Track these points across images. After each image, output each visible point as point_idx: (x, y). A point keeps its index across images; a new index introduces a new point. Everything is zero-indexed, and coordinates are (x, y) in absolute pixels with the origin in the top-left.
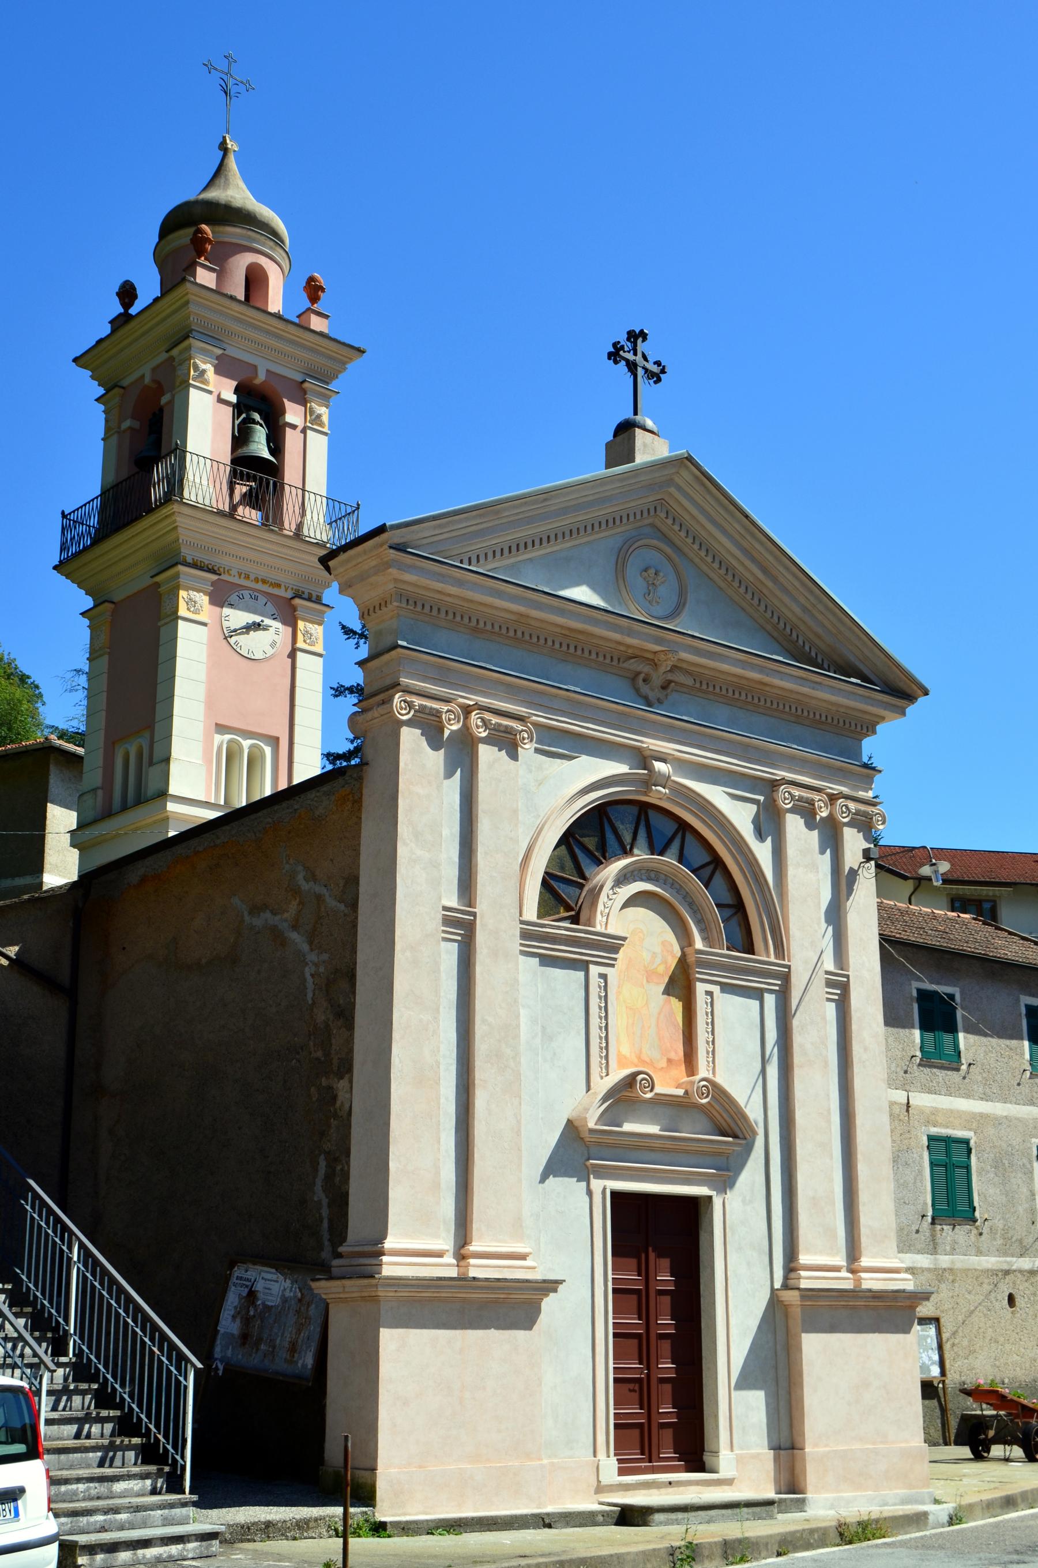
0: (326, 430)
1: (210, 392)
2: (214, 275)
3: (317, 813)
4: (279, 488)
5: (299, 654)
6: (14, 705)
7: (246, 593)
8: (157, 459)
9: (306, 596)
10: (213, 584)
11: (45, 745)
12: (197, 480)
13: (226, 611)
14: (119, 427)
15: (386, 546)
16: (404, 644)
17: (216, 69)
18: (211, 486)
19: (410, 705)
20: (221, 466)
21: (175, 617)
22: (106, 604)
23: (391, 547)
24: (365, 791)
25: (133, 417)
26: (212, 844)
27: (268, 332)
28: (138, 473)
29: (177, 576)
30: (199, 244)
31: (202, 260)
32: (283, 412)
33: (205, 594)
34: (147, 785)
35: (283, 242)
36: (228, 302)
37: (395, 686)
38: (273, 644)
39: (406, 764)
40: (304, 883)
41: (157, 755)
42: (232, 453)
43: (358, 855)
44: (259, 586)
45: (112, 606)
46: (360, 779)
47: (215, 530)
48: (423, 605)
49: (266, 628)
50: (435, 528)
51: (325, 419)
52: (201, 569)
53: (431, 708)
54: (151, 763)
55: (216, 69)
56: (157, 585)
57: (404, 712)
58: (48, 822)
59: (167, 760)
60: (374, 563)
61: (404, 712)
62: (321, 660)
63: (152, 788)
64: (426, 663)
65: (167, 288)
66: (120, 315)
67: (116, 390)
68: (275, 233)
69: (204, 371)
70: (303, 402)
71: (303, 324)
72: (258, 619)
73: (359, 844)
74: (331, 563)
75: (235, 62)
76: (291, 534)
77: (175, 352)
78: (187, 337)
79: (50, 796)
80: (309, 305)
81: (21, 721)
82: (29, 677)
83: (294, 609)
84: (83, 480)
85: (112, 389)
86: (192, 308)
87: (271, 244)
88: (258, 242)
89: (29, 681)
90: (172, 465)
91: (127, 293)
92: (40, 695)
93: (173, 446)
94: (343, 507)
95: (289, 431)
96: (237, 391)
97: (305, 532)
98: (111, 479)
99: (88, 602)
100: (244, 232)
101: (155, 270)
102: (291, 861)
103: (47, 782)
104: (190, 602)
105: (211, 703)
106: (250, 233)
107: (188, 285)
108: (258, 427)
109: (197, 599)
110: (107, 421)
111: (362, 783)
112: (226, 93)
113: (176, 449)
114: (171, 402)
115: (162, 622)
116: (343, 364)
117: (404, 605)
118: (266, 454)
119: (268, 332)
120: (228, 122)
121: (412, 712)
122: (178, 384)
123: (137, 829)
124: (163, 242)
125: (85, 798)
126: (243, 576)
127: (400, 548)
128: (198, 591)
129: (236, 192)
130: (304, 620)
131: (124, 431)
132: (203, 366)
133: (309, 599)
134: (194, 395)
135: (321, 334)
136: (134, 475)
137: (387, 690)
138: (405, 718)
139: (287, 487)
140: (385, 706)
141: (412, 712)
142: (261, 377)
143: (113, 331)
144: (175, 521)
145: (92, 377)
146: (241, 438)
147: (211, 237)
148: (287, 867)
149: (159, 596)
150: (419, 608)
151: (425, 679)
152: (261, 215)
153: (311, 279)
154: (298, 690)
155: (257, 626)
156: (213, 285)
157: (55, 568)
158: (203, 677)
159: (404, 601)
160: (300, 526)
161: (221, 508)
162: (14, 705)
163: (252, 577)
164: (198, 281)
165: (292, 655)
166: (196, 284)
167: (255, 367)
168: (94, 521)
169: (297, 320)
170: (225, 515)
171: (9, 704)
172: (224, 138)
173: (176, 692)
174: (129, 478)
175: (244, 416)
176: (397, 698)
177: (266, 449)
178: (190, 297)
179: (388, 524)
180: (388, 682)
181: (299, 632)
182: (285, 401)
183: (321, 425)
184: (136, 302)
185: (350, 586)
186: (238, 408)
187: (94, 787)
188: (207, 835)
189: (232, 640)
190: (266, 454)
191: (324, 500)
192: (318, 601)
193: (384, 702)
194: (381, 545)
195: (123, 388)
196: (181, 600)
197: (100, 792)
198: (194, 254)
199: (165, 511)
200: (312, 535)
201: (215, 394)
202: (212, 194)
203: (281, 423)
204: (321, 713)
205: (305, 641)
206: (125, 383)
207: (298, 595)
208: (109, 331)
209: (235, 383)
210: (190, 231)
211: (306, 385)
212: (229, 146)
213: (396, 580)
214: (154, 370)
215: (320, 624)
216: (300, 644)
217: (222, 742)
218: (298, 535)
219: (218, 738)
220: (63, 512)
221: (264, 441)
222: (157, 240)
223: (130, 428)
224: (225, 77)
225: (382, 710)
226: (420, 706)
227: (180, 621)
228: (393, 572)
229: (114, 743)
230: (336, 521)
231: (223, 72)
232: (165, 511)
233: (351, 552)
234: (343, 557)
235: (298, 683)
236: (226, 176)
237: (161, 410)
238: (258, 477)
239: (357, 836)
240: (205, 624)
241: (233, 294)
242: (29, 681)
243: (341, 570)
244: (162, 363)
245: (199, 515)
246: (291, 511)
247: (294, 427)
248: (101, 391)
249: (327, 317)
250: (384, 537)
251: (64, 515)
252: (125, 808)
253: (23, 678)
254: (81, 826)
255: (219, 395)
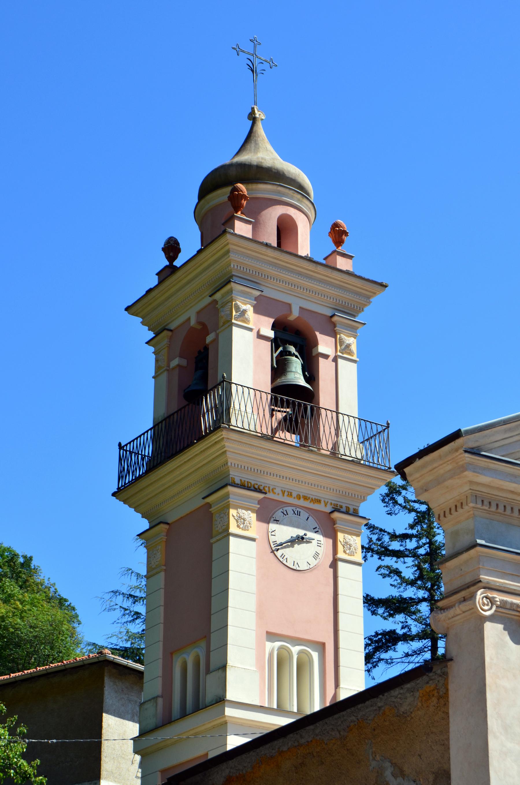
0: (355, 358)
1: (251, 330)
2: (250, 227)
3: (402, 709)
4: (316, 412)
5: (340, 564)
6: (56, 627)
7: (289, 509)
8: (205, 392)
9: (344, 509)
10: (260, 502)
11: (101, 659)
12: (243, 409)
13: (273, 526)
14: (168, 366)
15: (461, 451)
16: (483, 542)
17: (243, 51)
18: (255, 413)
19: (492, 601)
20: (264, 395)
21: (226, 534)
22: (162, 525)
23: (466, 451)
24: (451, 687)
25: (181, 356)
26: (296, 744)
27: (300, 274)
28: (188, 405)
29: (227, 496)
30: (235, 201)
31: (239, 214)
32: (316, 344)
33: (253, 511)
34: (205, 692)
35: (308, 194)
36: (264, 249)
37: (476, 583)
38: (317, 554)
39: (491, 659)
40: (392, 779)
41: (214, 663)
42: (271, 384)
43: (447, 748)
44: (302, 502)
45: (167, 527)
46: (445, 675)
47: (265, 454)
48: (497, 505)
49: (309, 541)
50: (506, 431)
51: (354, 348)
52: (248, 489)
53: (512, 604)
54: (208, 671)
55: (243, 51)
56: (209, 505)
57: (486, 608)
58: (104, 731)
59: (223, 667)
60: (450, 467)
61: (486, 608)
62: (360, 569)
63: (210, 695)
64: (503, 560)
65: (207, 242)
66: (166, 267)
67: (165, 333)
68: (301, 187)
69: (244, 312)
70: (333, 333)
71: (329, 264)
72: (301, 532)
73: (448, 739)
74: (407, 470)
75: (260, 44)
76: (328, 453)
77: (218, 296)
78: (229, 282)
79: (106, 706)
80: (334, 248)
81: (62, 640)
82: (66, 600)
83: (334, 522)
84: (138, 413)
85: (160, 331)
86: (232, 256)
87: (299, 196)
88: (284, 195)
89: (67, 604)
90: (220, 397)
91: (172, 248)
92: (77, 616)
93: (220, 379)
94: (374, 426)
95: (321, 360)
96: (274, 327)
97: (342, 451)
98: (163, 412)
99: (145, 524)
100: (274, 187)
101: (196, 227)
102: (378, 758)
103: (102, 694)
104: (240, 520)
105: (261, 613)
106: (280, 188)
107: (228, 236)
108: (294, 358)
109: (246, 517)
110: (157, 361)
111: (446, 680)
112: (253, 71)
113: (223, 382)
114: (216, 341)
115: (214, 540)
116: (368, 298)
117: (479, 506)
118: (302, 382)
119: (300, 274)
120: (255, 95)
121: (494, 608)
122: (221, 324)
123: (196, 735)
124: (202, 202)
125: (146, 706)
126: (286, 493)
127: (474, 452)
128: (247, 509)
129: (266, 153)
130: (343, 532)
131: (173, 369)
132: (243, 307)
133: (347, 513)
134: (236, 332)
135: (347, 273)
136: (184, 407)
137: (468, 587)
138: (488, 613)
139: (323, 412)
140: (467, 603)
141: (494, 608)
142: (295, 314)
143: (160, 282)
144: (224, 447)
145: (143, 323)
146: (279, 368)
147: (246, 193)
148: (374, 764)
149: (211, 516)
150: (493, 508)
151: (503, 575)
152: (289, 172)
153: (335, 225)
154: (341, 598)
155: (301, 539)
156: (250, 236)
157: (114, 494)
158: (253, 588)
159: (479, 502)
160: (336, 446)
161: (265, 432)
162: (56, 627)
163: (294, 494)
164: (237, 232)
165: (334, 565)
166: (236, 235)
167: (290, 305)
168: (148, 451)
169: (324, 262)
170: (269, 439)
171: (51, 625)
172: (253, 109)
173: (230, 604)
174: (180, 410)
175: (281, 349)
176: (480, 594)
177: (302, 378)
178: (230, 246)
179: (463, 430)
180: (468, 579)
181: (339, 543)
182: (317, 334)
183: (351, 353)
184: (180, 255)
185: (426, 490)
186: (276, 343)
187: (155, 695)
188: (291, 735)
189: (279, 554)
190: (302, 382)
191: (357, 420)
192: (355, 513)
193: (465, 600)
194: (457, 450)
195: (171, 331)
196: (231, 518)
197: (160, 701)
198: (232, 209)
199: (214, 437)
200: (348, 454)
201: (255, 331)
202: (245, 157)
203: (314, 354)
204: (362, 619)
205: (345, 552)
206: (172, 326)
207: (337, 509)
208: (156, 283)
209: (272, 321)
210: (228, 190)
211: (335, 319)
212: (257, 116)
213: (471, 482)
214: (198, 313)
215: (358, 535)
216: (341, 555)
217: (273, 650)
218: (334, 453)
219: (269, 646)
220: (120, 444)
221: (300, 371)
222: (197, 201)
223: (179, 366)
224: (251, 58)
225: (464, 607)
226: (502, 601)
227: (231, 539)
228: (469, 475)
229: (172, 654)
230: (367, 440)
231: (248, 53)
232: (214, 438)
233: (426, 459)
234: (418, 463)
235: (340, 591)
236: (256, 141)
237: (206, 348)
238: (296, 403)
239: (446, 731)
240: (253, 540)
241: (268, 242)
242: (67, 604)
243: (417, 475)
244: (206, 307)
245: (245, 439)
246: (327, 432)
247: (326, 357)
248: (151, 335)
249: (351, 257)
250: (459, 442)
251: (120, 447)
252: (184, 714)
253: (62, 602)
254: (143, 733)
255: (258, 332)
